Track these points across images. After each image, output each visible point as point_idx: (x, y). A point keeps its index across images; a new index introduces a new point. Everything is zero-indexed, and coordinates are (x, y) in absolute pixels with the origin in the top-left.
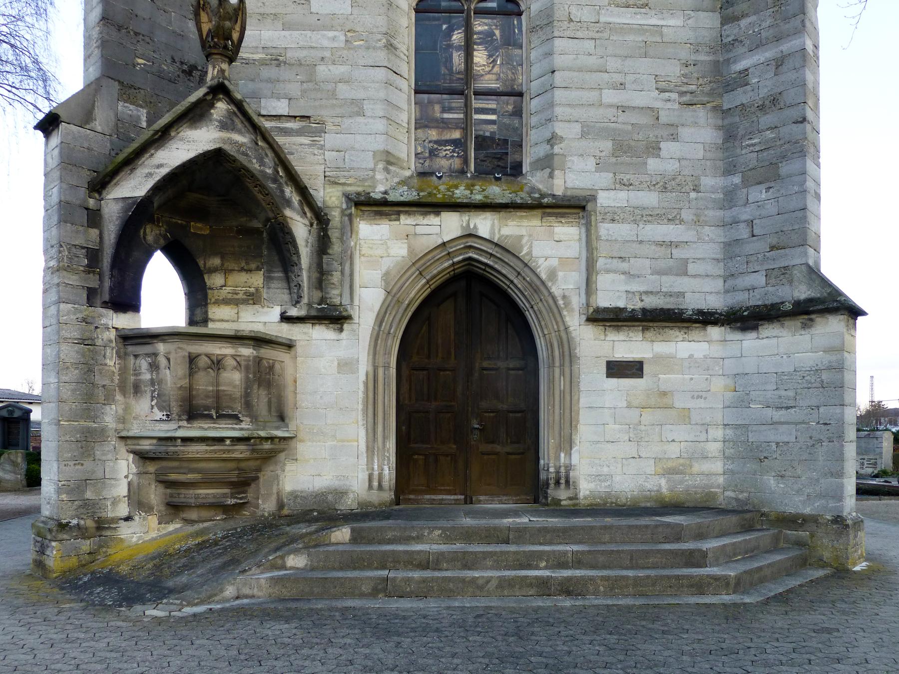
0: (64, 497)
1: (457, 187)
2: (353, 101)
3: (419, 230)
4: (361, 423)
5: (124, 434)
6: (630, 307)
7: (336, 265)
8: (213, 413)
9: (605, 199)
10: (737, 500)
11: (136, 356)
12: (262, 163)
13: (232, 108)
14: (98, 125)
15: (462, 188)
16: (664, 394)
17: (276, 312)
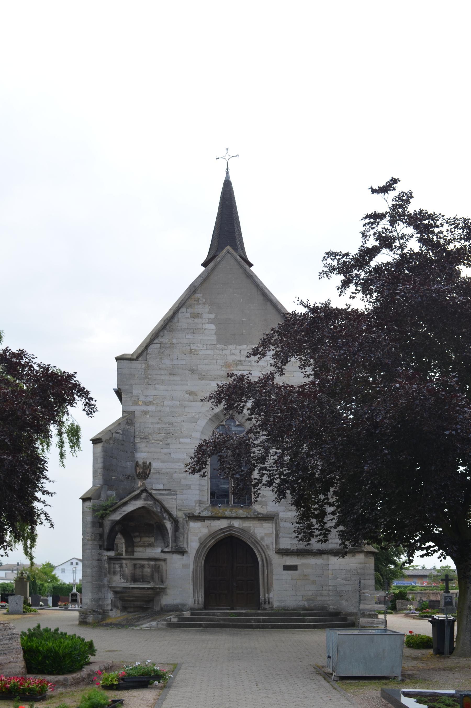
0: (93, 603)
1: (226, 511)
2: (187, 485)
3: (212, 524)
4: (191, 583)
5: (110, 586)
6: (292, 548)
7: (181, 535)
8: (141, 580)
9: (282, 515)
10: (334, 609)
11: (114, 564)
12: (156, 508)
13: (148, 494)
14: (102, 499)
15: (228, 511)
16: (306, 575)
17: (159, 550)
